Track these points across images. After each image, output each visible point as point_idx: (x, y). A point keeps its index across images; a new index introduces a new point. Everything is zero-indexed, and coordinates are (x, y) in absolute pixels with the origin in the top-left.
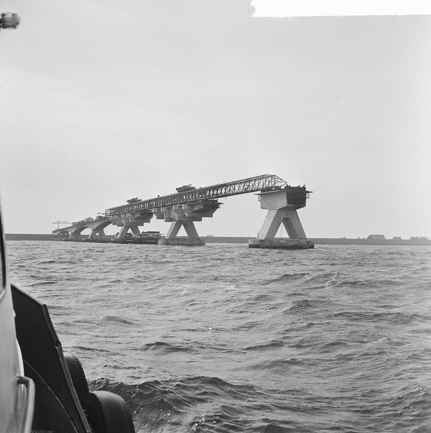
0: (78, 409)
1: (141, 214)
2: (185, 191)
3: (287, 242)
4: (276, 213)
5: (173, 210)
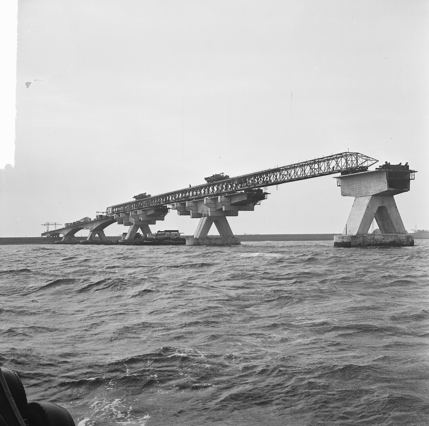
0: (18, 419)
1: (156, 211)
2: (218, 180)
3: (383, 237)
4: (369, 201)
5: (205, 202)
